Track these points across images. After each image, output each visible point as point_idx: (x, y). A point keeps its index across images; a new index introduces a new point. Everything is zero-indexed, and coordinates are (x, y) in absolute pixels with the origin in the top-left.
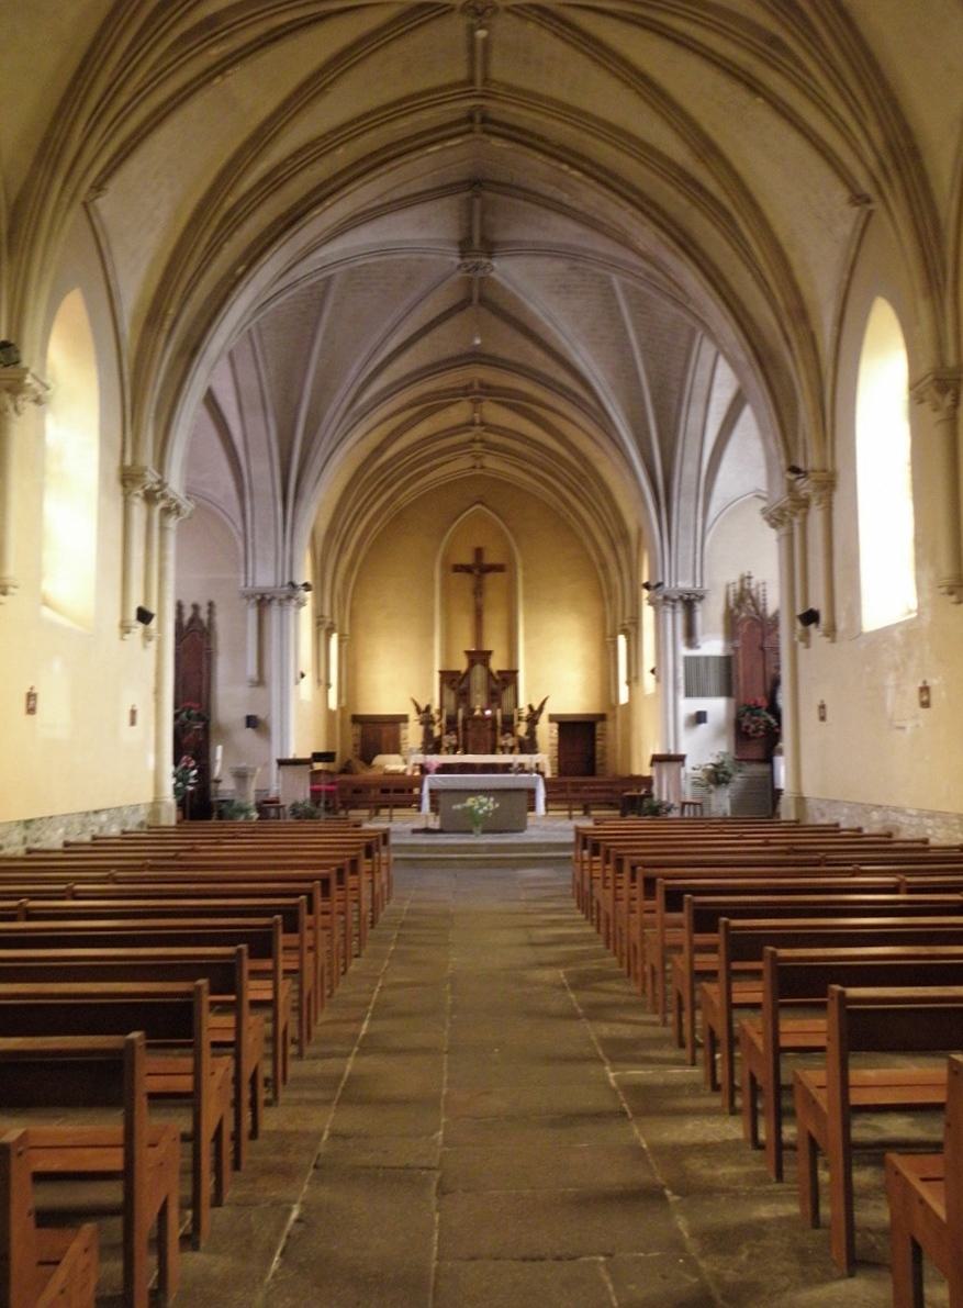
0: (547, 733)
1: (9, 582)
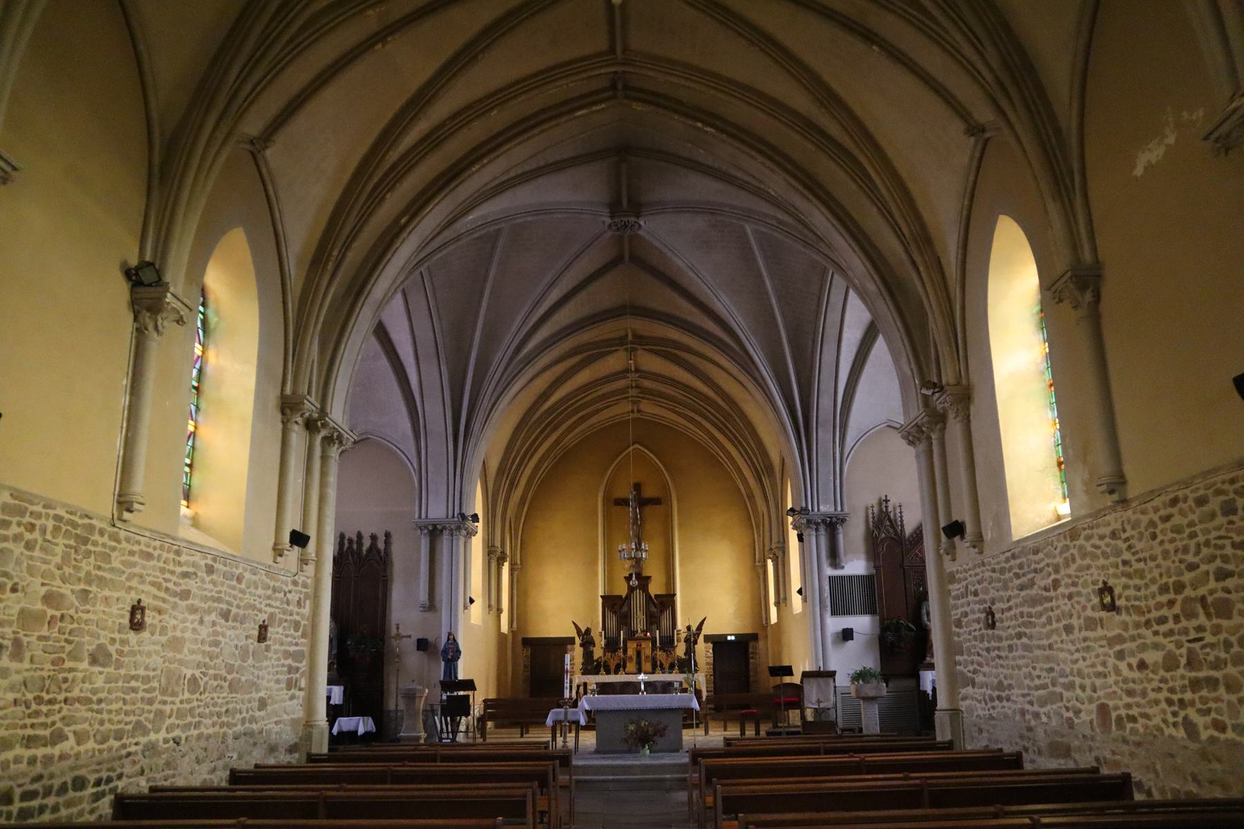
0: (703, 651)
1: (134, 498)
